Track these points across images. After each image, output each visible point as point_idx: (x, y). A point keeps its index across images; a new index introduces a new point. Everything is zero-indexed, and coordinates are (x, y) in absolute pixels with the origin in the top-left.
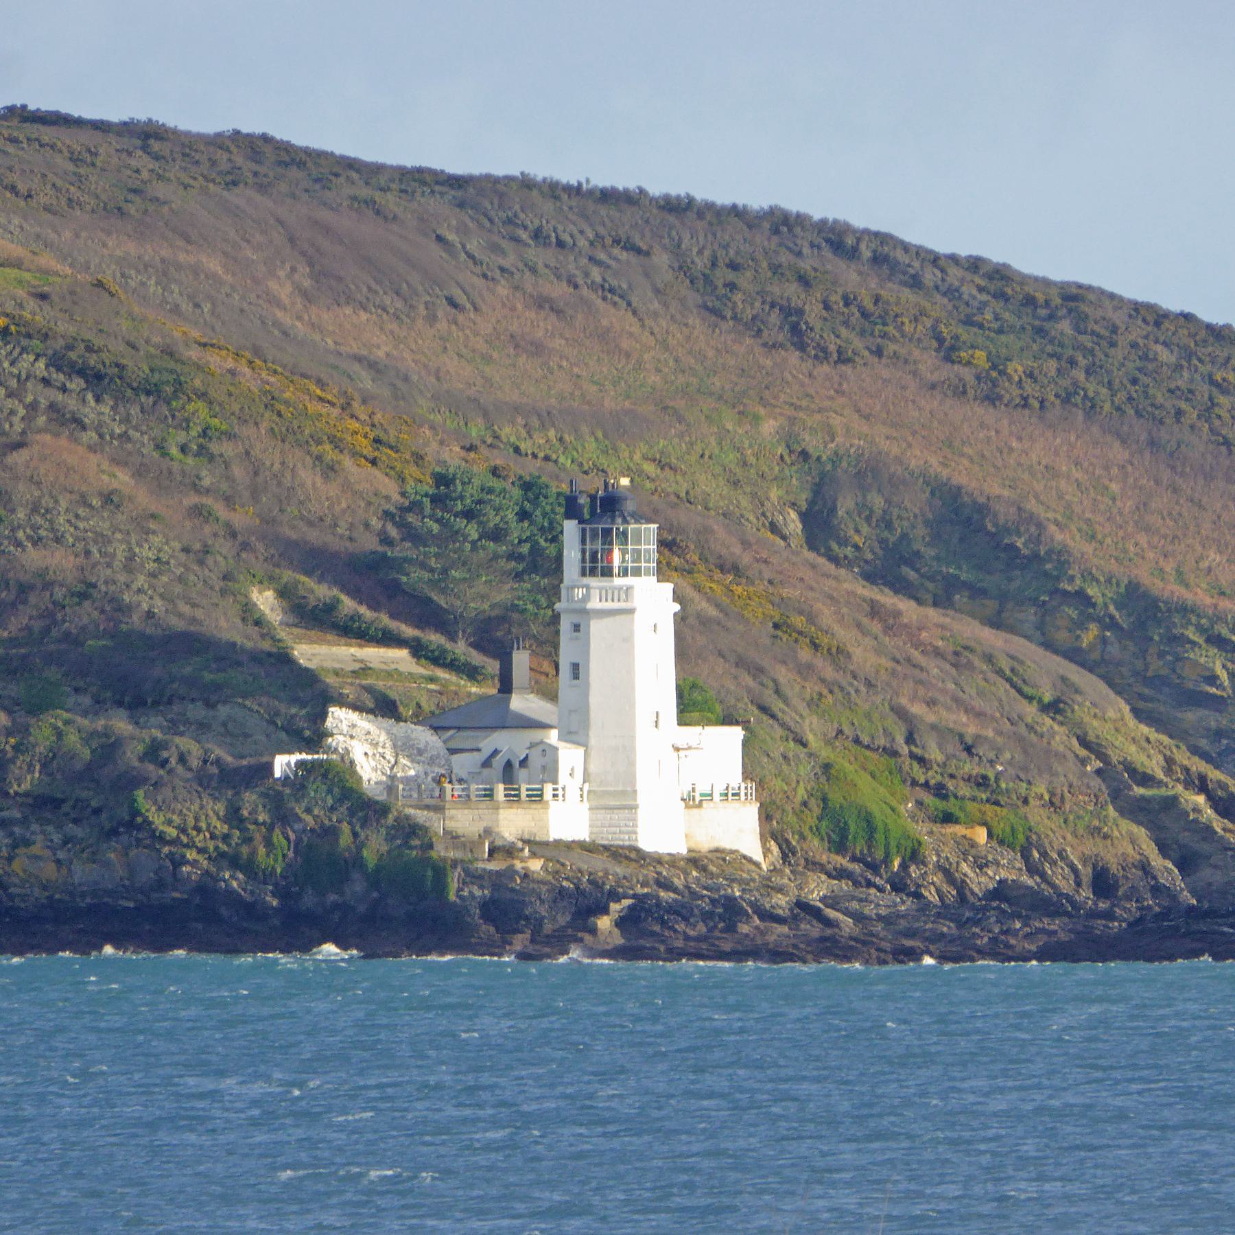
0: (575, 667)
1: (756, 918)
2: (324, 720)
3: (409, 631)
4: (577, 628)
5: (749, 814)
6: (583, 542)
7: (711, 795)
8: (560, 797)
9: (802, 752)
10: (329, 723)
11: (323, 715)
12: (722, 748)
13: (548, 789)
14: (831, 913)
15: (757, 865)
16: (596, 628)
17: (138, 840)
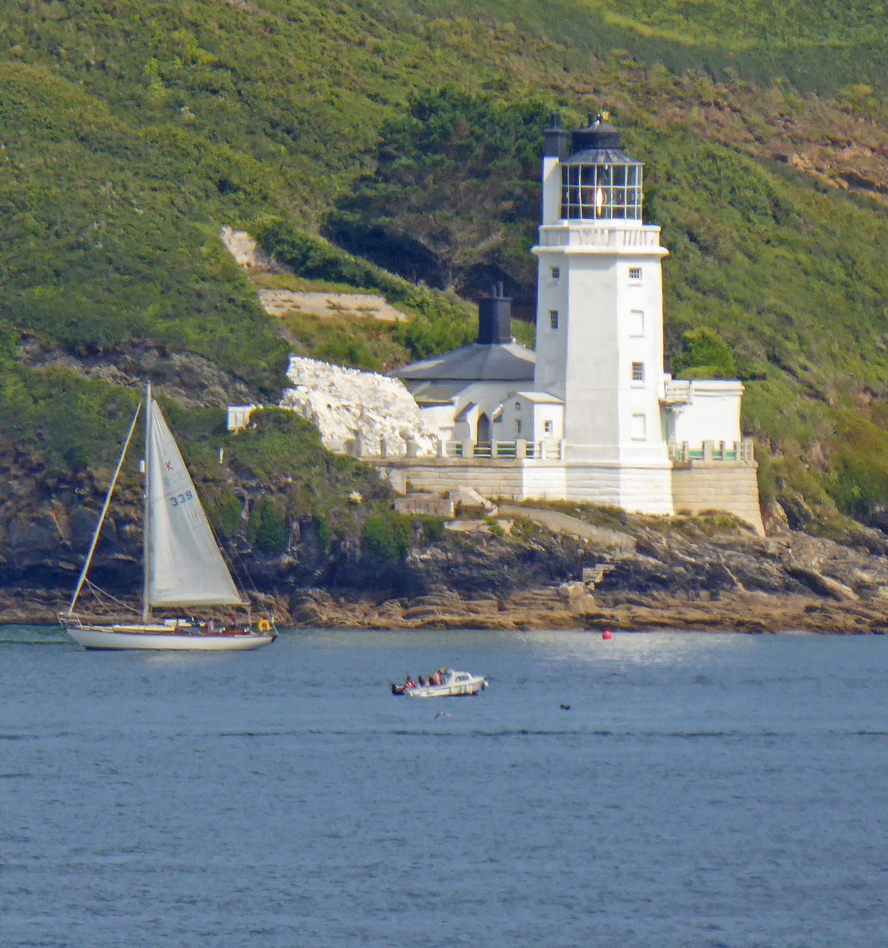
0: (554, 315)
1: (740, 585)
2: (286, 370)
3: (385, 274)
4: (556, 273)
5: (748, 481)
6: (564, 182)
7: (703, 453)
8: (536, 455)
9: (820, 410)
10: (291, 373)
11: (286, 364)
12: (715, 412)
13: (521, 446)
14: (830, 582)
15: (750, 528)
16: (577, 277)
17: (80, 497)
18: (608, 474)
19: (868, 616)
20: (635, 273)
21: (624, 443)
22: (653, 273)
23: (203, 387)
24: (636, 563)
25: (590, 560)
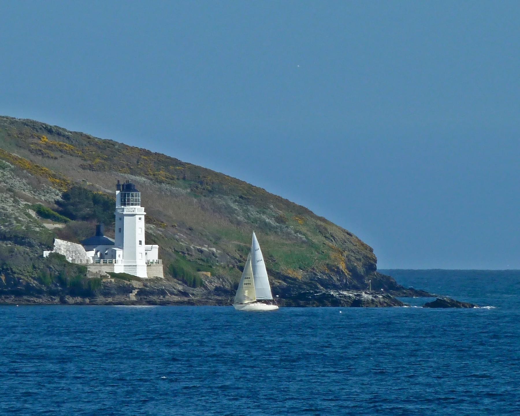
5: (161, 268)
12: (155, 249)
18: (134, 267)
19: (458, 331)
20: (140, 219)
21: (137, 260)
22: (143, 217)
23: (33, 246)
24: (144, 289)
25: (135, 289)
